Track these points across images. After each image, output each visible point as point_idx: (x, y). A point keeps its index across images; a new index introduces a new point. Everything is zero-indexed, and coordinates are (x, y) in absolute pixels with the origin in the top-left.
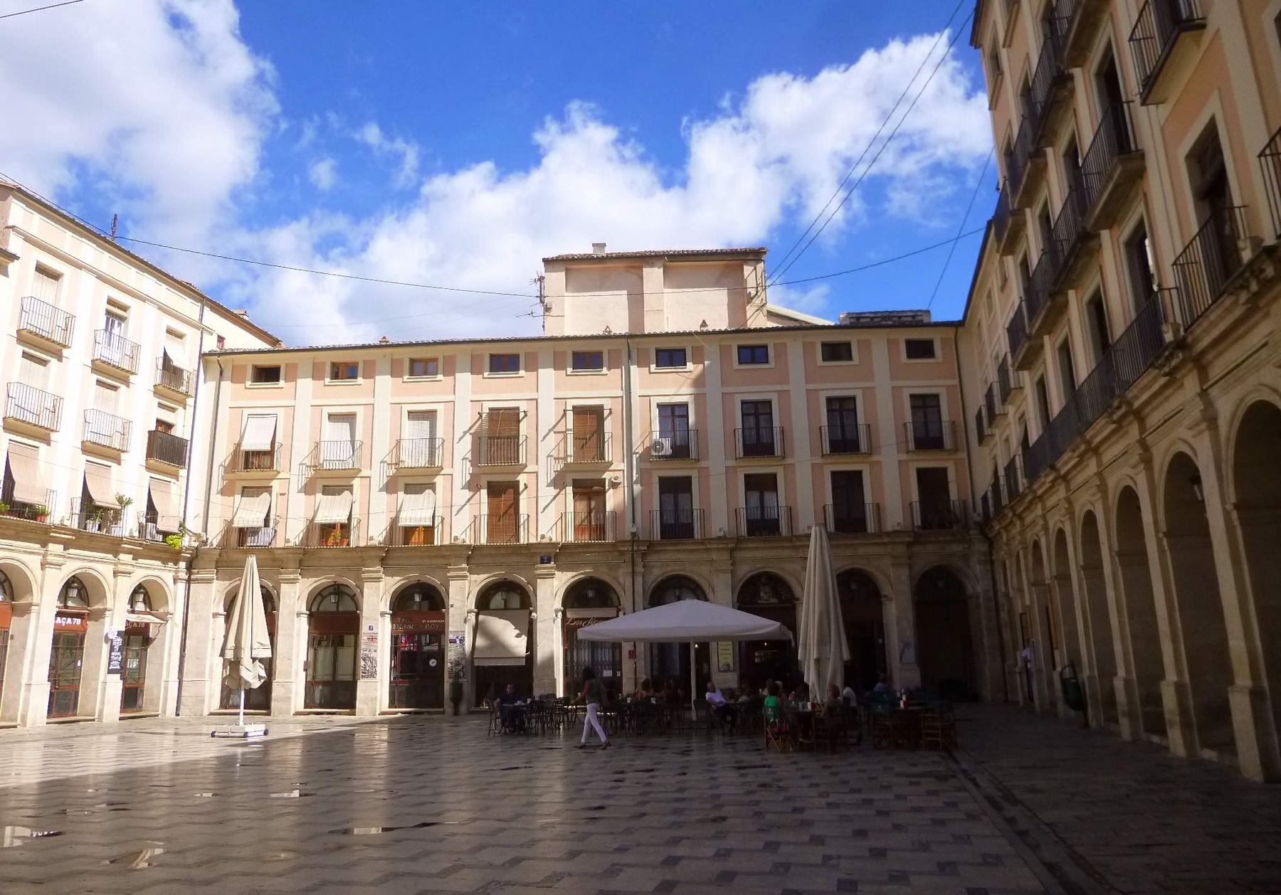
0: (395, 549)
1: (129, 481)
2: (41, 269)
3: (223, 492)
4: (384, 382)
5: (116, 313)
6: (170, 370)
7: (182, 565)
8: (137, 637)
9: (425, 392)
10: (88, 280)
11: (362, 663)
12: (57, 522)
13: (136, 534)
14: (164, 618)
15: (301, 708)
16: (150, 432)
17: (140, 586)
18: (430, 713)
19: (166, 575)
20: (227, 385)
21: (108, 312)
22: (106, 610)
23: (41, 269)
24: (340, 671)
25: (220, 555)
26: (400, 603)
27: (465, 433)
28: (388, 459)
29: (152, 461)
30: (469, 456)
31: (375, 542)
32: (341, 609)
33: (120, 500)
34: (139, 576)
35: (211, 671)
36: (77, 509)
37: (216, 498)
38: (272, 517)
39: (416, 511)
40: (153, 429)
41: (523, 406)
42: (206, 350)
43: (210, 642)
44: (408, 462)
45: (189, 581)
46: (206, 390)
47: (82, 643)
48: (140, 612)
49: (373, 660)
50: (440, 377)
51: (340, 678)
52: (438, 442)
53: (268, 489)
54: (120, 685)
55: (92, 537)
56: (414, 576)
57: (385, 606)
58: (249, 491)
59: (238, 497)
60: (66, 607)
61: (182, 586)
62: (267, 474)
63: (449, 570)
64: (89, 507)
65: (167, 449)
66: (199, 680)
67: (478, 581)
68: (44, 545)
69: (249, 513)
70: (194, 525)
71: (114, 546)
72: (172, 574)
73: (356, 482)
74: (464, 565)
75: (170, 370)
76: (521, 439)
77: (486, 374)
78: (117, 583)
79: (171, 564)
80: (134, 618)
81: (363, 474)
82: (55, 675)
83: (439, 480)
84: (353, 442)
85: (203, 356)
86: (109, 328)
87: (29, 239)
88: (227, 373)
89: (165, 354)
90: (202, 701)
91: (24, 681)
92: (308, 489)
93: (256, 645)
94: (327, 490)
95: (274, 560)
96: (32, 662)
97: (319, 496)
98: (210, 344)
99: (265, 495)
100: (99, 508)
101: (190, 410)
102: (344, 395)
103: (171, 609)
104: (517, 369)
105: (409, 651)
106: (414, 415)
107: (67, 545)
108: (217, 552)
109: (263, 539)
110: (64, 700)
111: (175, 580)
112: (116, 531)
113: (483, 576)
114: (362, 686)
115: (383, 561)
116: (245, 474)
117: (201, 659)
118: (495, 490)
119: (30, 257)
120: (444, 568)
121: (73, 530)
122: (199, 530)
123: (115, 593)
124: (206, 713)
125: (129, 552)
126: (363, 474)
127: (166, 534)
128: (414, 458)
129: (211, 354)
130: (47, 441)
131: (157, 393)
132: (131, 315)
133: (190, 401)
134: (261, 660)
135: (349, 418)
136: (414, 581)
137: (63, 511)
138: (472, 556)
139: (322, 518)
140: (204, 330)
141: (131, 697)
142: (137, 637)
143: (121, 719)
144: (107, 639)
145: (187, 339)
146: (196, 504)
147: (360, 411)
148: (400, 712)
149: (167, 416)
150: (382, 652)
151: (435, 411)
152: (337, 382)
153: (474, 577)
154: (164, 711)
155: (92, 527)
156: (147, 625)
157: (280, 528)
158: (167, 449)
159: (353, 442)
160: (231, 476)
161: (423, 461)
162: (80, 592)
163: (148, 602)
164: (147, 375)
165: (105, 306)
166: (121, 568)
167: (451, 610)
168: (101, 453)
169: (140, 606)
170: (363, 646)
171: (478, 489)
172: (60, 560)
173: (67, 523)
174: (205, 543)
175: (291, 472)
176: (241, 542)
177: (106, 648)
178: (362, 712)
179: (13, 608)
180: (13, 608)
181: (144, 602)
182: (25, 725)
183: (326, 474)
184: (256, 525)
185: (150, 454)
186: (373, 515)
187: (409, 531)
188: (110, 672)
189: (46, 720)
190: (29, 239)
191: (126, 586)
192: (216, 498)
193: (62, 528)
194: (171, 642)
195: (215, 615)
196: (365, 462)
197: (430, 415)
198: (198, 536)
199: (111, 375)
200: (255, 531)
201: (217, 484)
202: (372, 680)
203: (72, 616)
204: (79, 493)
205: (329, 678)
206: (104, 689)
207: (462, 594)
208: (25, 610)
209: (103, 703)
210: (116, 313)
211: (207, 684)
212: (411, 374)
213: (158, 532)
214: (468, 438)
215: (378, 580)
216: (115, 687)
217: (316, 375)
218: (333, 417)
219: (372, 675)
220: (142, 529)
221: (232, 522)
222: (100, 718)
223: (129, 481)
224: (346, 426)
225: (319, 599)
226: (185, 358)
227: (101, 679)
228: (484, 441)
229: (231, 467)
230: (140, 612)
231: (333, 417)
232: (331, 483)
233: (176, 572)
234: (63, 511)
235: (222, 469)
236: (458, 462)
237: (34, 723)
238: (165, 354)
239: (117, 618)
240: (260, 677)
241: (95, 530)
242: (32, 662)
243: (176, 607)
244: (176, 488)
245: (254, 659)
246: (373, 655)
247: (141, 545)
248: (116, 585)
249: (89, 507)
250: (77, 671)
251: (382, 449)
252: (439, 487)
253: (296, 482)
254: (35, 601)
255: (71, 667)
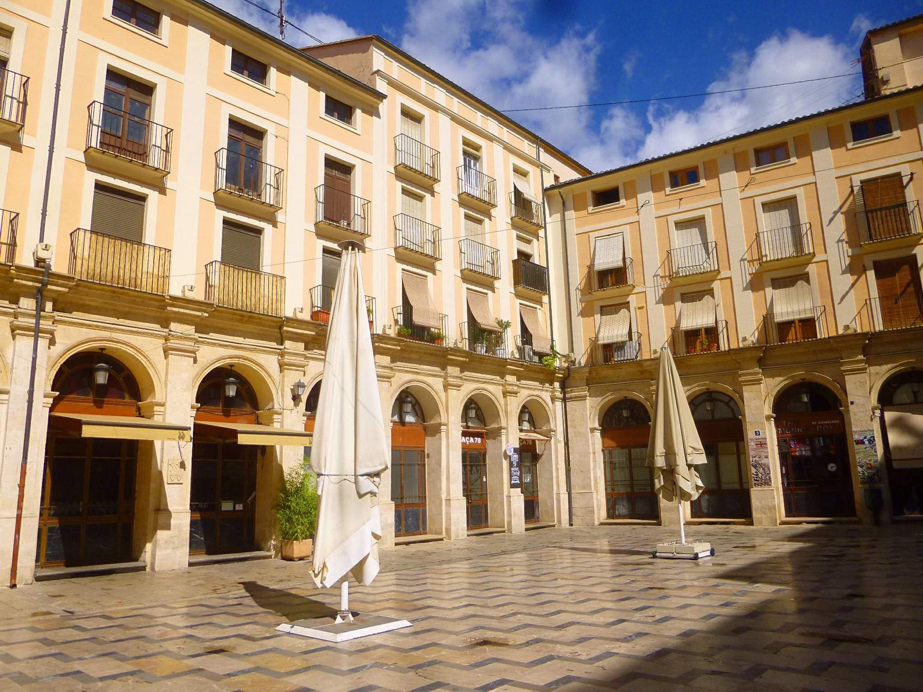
0: (774, 347)
1: (503, 304)
2: (407, 113)
3: (583, 314)
4: (730, 179)
5: (471, 154)
6: (521, 202)
7: (557, 385)
8: (529, 454)
9: (777, 181)
10: (444, 120)
11: (753, 470)
12: (451, 345)
13: (517, 356)
14: (548, 434)
15: (689, 519)
16: (514, 261)
17: (524, 407)
18: (841, 523)
19: (545, 394)
20: (571, 214)
21: (465, 153)
22: (501, 428)
23: (407, 113)
24: (724, 479)
25: (590, 372)
26: (783, 407)
27: (835, 213)
28: (660, 272)
29: (520, 288)
30: (844, 237)
31: (748, 343)
32: (717, 417)
33: (500, 323)
34: (524, 395)
35: (596, 483)
36: (466, 335)
37: (578, 321)
38: (634, 329)
39: (788, 306)
40: (516, 257)
41: (905, 170)
42: (547, 185)
43: (591, 456)
44: (770, 254)
45: (564, 400)
46: (552, 222)
47: (484, 461)
48: (527, 431)
49: (766, 468)
50: (793, 160)
51: (725, 487)
52: (804, 229)
53: (626, 305)
54: (522, 497)
55: (481, 359)
56: (800, 374)
57: (768, 410)
58: (608, 309)
59: (598, 317)
60: (468, 427)
61: (559, 405)
62: (622, 290)
63: (842, 364)
64: (477, 332)
65: (530, 277)
66: (587, 492)
67: (881, 373)
68: (444, 368)
69: (613, 330)
70: (561, 347)
71: (500, 368)
72: (549, 394)
73: (716, 285)
74: (861, 357)
75: (521, 202)
76: (911, 207)
77: (850, 145)
78: (509, 399)
79: (547, 385)
80: (523, 435)
81: (724, 274)
82: (468, 491)
83: (812, 269)
84: (705, 244)
85: (545, 191)
86: (467, 167)
87: (392, 83)
88: (569, 203)
89: (515, 187)
90: (593, 512)
91: (444, 497)
92: (666, 299)
93: (689, 450)
94: (686, 298)
95: (642, 372)
96: (448, 478)
97: (679, 304)
98: (549, 182)
99: (624, 311)
100: (484, 330)
101: (542, 241)
102: (692, 201)
103: (552, 427)
104: (889, 131)
105: (801, 457)
106: (768, 207)
107: (463, 367)
108: (587, 370)
109: (630, 353)
110: (477, 515)
111: (553, 399)
112: (500, 354)
113: (885, 367)
114: (757, 496)
115: (761, 362)
116: (601, 294)
117: (586, 472)
118: (884, 270)
119: (394, 102)
120: (837, 362)
121: (466, 352)
122: (566, 352)
123: (506, 412)
124: (597, 523)
125: (513, 373)
126: (724, 274)
127: (541, 355)
128: (778, 248)
129: (552, 187)
130: (433, 270)
131: (515, 226)
132: (484, 154)
133: (541, 233)
134: (697, 468)
135: (698, 223)
136: (798, 380)
137: (454, 333)
138: (869, 346)
139: (688, 324)
140: (542, 167)
141: (531, 509)
142: (529, 454)
143: (527, 530)
144: (506, 456)
145: (531, 175)
146: (562, 328)
147: (709, 214)
148: (805, 524)
149: (525, 248)
150: (774, 458)
151: (794, 198)
152: (678, 189)
153: (873, 369)
154: (560, 522)
155: (481, 350)
156: (534, 441)
157: (644, 340)
158: (530, 277)
159: (705, 244)
160: (589, 297)
161: (789, 251)
162: (478, 412)
163: (531, 421)
164: (503, 211)
165: (461, 147)
166: (509, 388)
167: (851, 407)
168: (478, 279)
169: (526, 426)
170: (752, 453)
171: (865, 270)
172: (458, 382)
173: (460, 345)
174: (573, 362)
175: (647, 284)
176: (607, 359)
177: (505, 464)
178: (761, 523)
179: (425, 429)
180: (425, 429)
181: (529, 422)
182: (450, 539)
183: (681, 281)
184: (620, 339)
185: (516, 283)
186: (740, 316)
187: (784, 327)
188: (513, 486)
189: (466, 533)
190: (392, 83)
191: (514, 406)
192: (578, 321)
193: (456, 351)
194: (557, 457)
195: (593, 430)
196: (724, 264)
197: (789, 203)
198: (567, 357)
199: (476, 208)
200: (620, 346)
201: (576, 307)
202: (766, 488)
203: (474, 435)
204: (465, 319)
205: (714, 486)
206: (509, 502)
207: (862, 391)
208: (435, 430)
209: (510, 515)
210: (471, 154)
211: (595, 495)
212: (758, 164)
213: (535, 353)
214: (841, 218)
215: (758, 382)
216: (518, 500)
217: (656, 187)
218: (680, 225)
219: (767, 482)
220: (520, 350)
221: (597, 338)
222: (510, 530)
223: (503, 304)
224: (695, 231)
225: (727, 399)
226: (532, 192)
227: (506, 493)
228: (862, 218)
229: (587, 290)
230: (527, 431)
231: (680, 225)
232: (689, 289)
233: (553, 392)
234: (454, 333)
235: (579, 293)
236: (833, 246)
237: (457, 536)
238: (515, 187)
239: (511, 438)
240: (698, 487)
241: (483, 351)
242: (448, 478)
243: (558, 425)
244: (541, 314)
245: (689, 466)
246: (764, 461)
247: (522, 366)
248: (506, 405)
249: (477, 332)
250: (484, 486)
251: (739, 246)
252: (813, 277)
253: (653, 295)
254: (443, 420)
255: (479, 482)
